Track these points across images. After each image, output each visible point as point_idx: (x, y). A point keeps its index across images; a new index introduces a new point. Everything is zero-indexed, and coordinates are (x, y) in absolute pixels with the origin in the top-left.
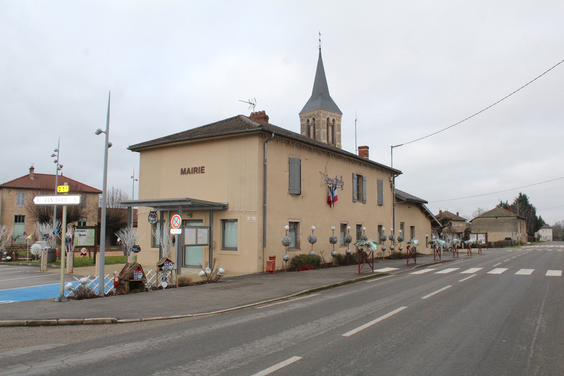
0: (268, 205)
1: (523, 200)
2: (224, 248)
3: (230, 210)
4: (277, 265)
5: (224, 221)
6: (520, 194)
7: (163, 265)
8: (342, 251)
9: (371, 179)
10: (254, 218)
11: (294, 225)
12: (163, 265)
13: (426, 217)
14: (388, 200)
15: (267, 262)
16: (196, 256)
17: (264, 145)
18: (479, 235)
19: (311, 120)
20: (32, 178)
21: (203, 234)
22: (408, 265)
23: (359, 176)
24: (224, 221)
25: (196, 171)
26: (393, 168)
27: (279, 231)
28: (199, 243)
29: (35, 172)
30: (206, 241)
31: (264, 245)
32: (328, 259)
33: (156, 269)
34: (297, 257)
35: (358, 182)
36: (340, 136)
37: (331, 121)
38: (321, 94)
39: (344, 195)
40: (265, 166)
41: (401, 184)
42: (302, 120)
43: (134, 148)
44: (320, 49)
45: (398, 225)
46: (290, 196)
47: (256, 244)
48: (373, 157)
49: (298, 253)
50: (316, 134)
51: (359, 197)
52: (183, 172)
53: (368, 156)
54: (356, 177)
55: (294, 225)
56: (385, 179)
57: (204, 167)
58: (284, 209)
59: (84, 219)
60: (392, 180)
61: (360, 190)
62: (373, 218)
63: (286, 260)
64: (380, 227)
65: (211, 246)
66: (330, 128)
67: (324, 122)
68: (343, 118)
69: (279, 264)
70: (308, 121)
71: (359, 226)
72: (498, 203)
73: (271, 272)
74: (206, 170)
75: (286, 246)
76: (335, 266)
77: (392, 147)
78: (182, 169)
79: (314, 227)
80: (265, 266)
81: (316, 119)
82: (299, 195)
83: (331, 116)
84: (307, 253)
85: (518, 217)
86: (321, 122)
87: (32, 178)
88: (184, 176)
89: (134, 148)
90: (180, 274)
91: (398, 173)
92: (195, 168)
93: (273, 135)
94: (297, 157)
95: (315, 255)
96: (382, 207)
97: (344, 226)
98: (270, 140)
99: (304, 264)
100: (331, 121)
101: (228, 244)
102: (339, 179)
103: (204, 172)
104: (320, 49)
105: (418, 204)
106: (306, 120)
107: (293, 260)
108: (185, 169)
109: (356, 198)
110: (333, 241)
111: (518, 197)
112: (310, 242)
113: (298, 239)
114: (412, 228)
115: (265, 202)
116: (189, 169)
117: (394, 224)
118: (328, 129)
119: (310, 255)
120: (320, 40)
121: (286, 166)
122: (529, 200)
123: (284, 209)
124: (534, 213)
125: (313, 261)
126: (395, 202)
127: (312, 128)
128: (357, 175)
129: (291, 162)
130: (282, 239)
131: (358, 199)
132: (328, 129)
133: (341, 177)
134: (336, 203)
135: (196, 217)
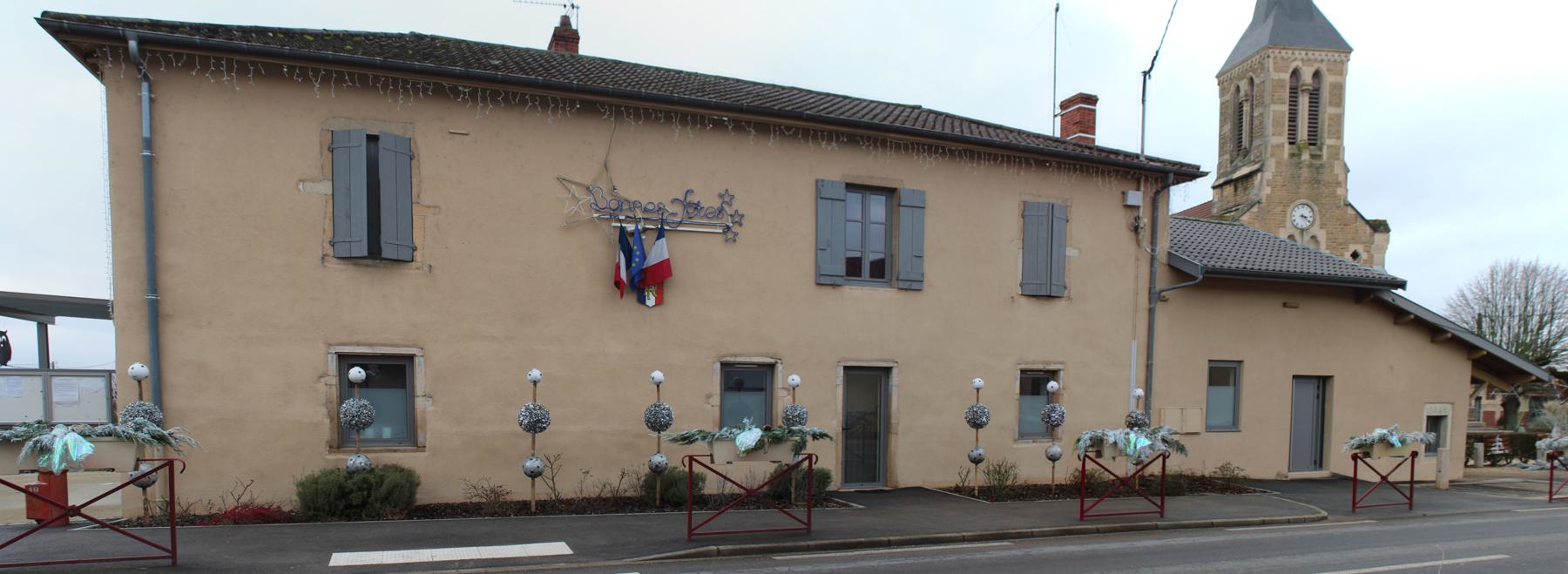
19: (1244, 85)
22: (692, 537)
26: (1148, 153)
36: (1338, 120)
37: (1307, 76)
42: (1222, 93)
48: (1114, 132)
50: (1256, 122)
53: (1091, 128)
66: (1304, 102)
67: (1279, 84)
68: (1354, 65)
70: (1238, 89)
79: (536, 373)
81: (1256, 81)
83: (1306, 62)
86: (1268, 86)
93: (133, 44)
100: (1307, 76)
106: (1233, 89)
117: (1149, 368)
118: (1293, 103)
127: (1246, 108)
132: (1293, 103)
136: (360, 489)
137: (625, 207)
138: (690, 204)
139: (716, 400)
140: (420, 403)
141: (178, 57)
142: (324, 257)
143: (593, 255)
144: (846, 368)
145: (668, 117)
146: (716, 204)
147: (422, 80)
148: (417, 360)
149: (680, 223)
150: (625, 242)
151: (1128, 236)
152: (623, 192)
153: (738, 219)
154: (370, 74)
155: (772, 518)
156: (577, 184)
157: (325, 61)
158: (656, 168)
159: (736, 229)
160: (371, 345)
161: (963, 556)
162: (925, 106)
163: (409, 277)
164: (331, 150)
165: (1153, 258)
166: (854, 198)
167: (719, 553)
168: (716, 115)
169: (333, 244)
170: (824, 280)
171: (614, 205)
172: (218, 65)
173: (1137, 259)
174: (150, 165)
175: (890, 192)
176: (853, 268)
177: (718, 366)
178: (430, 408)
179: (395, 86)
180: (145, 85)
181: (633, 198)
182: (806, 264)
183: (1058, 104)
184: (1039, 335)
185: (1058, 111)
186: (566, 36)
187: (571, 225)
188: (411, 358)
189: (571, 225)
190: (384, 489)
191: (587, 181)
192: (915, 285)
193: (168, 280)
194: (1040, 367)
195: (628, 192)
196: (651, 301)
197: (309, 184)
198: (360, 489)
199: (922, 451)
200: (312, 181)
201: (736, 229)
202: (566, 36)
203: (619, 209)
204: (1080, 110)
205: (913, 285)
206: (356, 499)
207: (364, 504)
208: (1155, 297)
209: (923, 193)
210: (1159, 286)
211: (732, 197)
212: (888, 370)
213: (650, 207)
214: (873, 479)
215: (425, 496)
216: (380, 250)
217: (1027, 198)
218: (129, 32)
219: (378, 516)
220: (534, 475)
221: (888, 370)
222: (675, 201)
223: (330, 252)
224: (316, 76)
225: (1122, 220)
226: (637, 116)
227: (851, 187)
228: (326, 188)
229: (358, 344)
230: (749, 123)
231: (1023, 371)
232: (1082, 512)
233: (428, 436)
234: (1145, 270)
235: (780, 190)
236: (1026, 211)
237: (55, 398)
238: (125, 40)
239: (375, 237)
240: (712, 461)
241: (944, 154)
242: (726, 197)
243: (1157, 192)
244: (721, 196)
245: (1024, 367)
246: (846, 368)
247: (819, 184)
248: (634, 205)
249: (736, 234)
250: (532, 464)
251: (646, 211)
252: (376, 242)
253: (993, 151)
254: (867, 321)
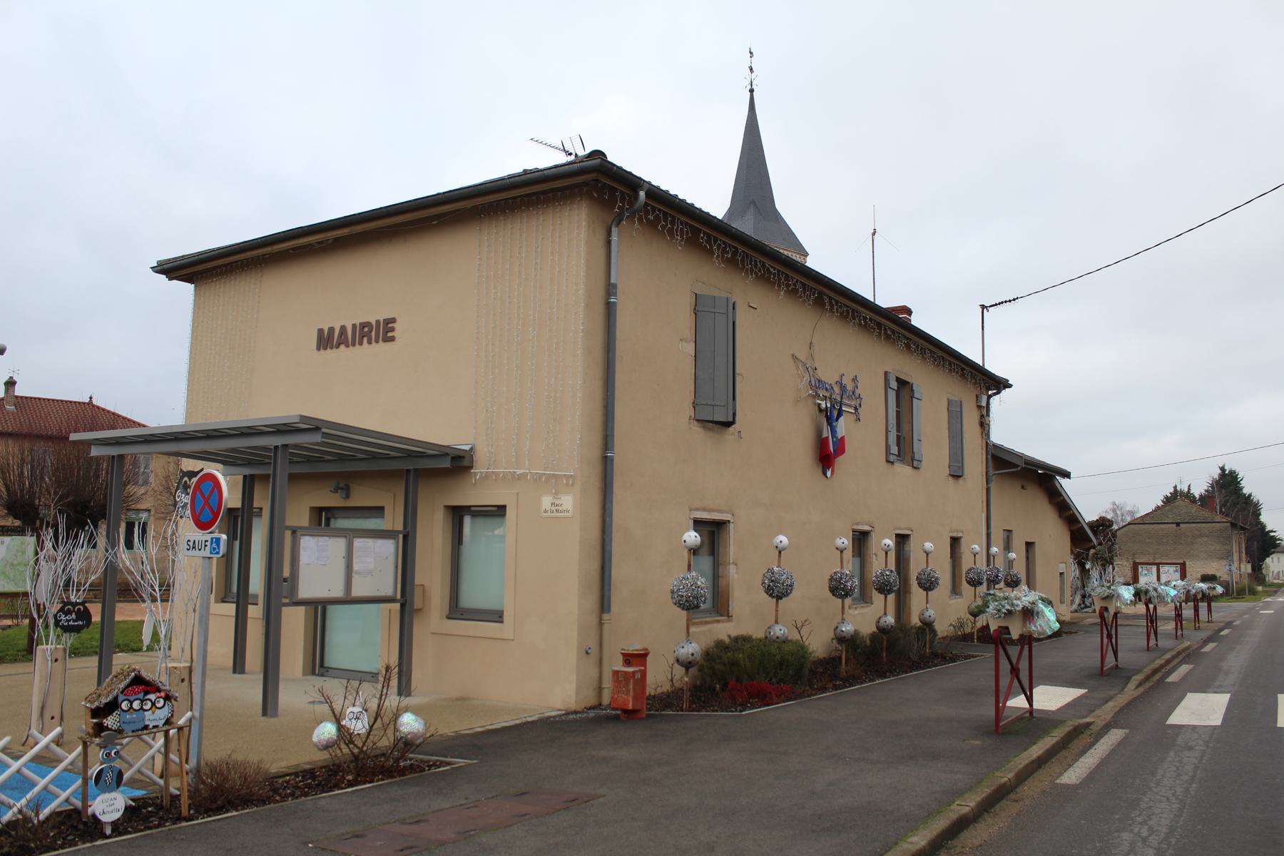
0: (620, 453)
1: (1228, 482)
2: (456, 611)
3: (479, 470)
4: (650, 679)
5: (457, 514)
6: (1222, 469)
7: (113, 706)
8: (863, 619)
9: (934, 394)
10: (567, 502)
11: (713, 531)
12: (113, 706)
13: (1060, 516)
14: (975, 464)
15: (616, 673)
16: (360, 640)
17: (609, 233)
18: (1163, 569)
20: (10, 408)
21: (376, 562)
23: (902, 383)
24: (457, 514)
25: (368, 335)
27: (659, 552)
28: (357, 592)
29: (19, 391)
30: (386, 584)
31: (604, 604)
32: (818, 643)
33: (85, 724)
34: (719, 644)
35: (898, 406)
38: (753, 202)
39: (864, 434)
40: (610, 311)
41: (1012, 425)
43: (174, 269)
44: (752, 91)
45: (998, 536)
46: (696, 428)
47: (570, 598)
49: (724, 630)
51: (903, 449)
52: (326, 340)
54: (894, 385)
55: (713, 531)
56: (965, 394)
57: (393, 320)
58: (674, 477)
59: (144, 516)
60: (984, 404)
61: (905, 427)
62: (934, 511)
63: (687, 665)
64: (955, 541)
65: (406, 602)
69: (659, 676)
71: (902, 539)
72: (1168, 491)
73: (630, 714)
74: (399, 330)
75: (688, 609)
76: (850, 680)
77: (983, 307)
78: (321, 331)
79: (783, 539)
80: (608, 683)
82: (728, 424)
84: (758, 634)
85: (1233, 525)
87: (10, 408)
88: (330, 353)
89: (174, 269)
90: (275, 714)
91: (1000, 384)
92: (363, 325)
93: (642, 194)
94: (724, 295)
95: (786, 641)
96: (961, 481)
97: (861, 539)
98: (631, 217)
99: (743, 679)
101: (472, 596)
102: (850, 387)
103: (392, 339)
104: (752, 91)
105: (1042, 480)
107: (707, 655)
108: (331, 330)
109: (894, 450)
110: (838, 589)
111: (1216, 477)
112: (769, 591)
113: (722, 582)
114: (1029, 545)
115: (603, 568)
116: (343, 328)
119: (767, 641)
120: (751, 69)
121: (684, 322)
122: (1243, 483)
123: (674, 477)
124: (1257, 514)
125: (782, 664)
126: (991, 469)
128: (898, 380)
129: (700, 307)
130: (672, 582)
131: (899, 455)
133: (855, 379)
134: (840, 461)
135: (363, 496)
196: (829, 474)
228: (690, 348)
237: (356, 567)
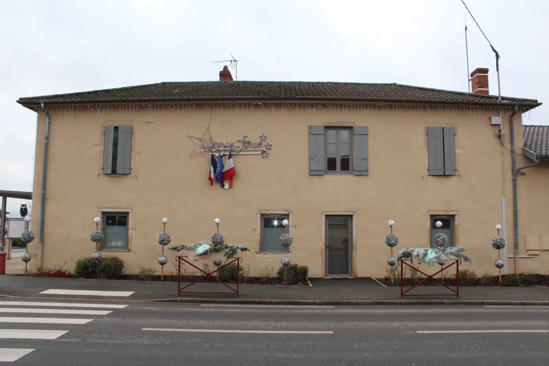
26: (503, 95)
53: (486, 85)
93: (42, 105)
136: (92, 266)
137: (216, 146)
138: (245, 142)
139: (258, 232)
140: (130, 232)
141: (56, 107)
142: (99, 175)
143: (206, 167)
144: (326, 216)
145: (233, 106)
146: (258, 141)
147: (134, 104)
148: (130, 214)
149: (240, 151)
150: (214, 162)
151: (495, 142)
152: (215, 140)
153: (269, 147)
154: (116, 104)
155: (220, 288)
156: (196, 138)
157: (100, 102)
158: (229, 127)
159: (268, 151)
160: (113, 208)
161: (227, 310)
162: (398, 83)
163: (129, 180)
164: (104, 134)
165: (512, 152)
166: (332, 133)
167: (181, 301)
168: (255, 102)
169: (102, 169)
170: (314, 173)
171: (211, 145)
172: (68, 108)
173: (502, 153)
174: (47, 145)
175: (350, 128)
176: (331, 165)
177: (259, 215)
178: (134, 234)
179: (125, 107)
180: (48, 118)
181: (219, 142)
182: (304, 164)
183: (470, 74)
184: (442, 196)
185: (470, 78)
186: (225, 74)
187: (192, 155)
188: (128, 213)
189: (192, 155)
190: (101, 267)
191: (200, 136)
192: (363, 173)
193: (49, 186)
194: (443, 213)
195: (217, 139)
196: (227, 186)
197: (96, 147)
198: (92, 266)
199: (370, 259)
200: (98, 146)
201: (268, 151)
202: (225, 74)
203: (213, 146)
204: (480, 77)
205: (363, 173)
206: (90, 270)
207: (94, 272)
208: (516, 173)
209: (366, 128)
210: (518, 166)
211: (266, 137)
212: (351, 216)
213: (228, 145)
214: (347, 272)
215: (127, 271)
216: (116, 171)
217: (428, 126)
218: (41, 101)
219: (96, 278)
220: (162, 264)
221: (351, 216)
222: (238, 141)
223: (101, 172)
224: (98, 108)
225: (490, 133)
226: (220, 106)
227: (327, 128)
228: (102, 148)
229: (109, 208)
230: (271, 104)
231: (453, 216)
232: (402, 293)
233: (132, 246)
234: (508, 158)
235: (291, 133)
236: (428, 132)
238: (40, 104)
239: (116, 166)
240: (412, 263)
241: (374, 107)
242: (263, 138)
243: (512, 116)
244: (261, 137)
245: (432, 213)
246: (326, 216)
247: (310, 127)
248: (220, 145)
249: (268, 154)
250: (161, 259)
251: (225, 147)
252: (116, 166)
253: (404, 104)
254: (338, 192)
